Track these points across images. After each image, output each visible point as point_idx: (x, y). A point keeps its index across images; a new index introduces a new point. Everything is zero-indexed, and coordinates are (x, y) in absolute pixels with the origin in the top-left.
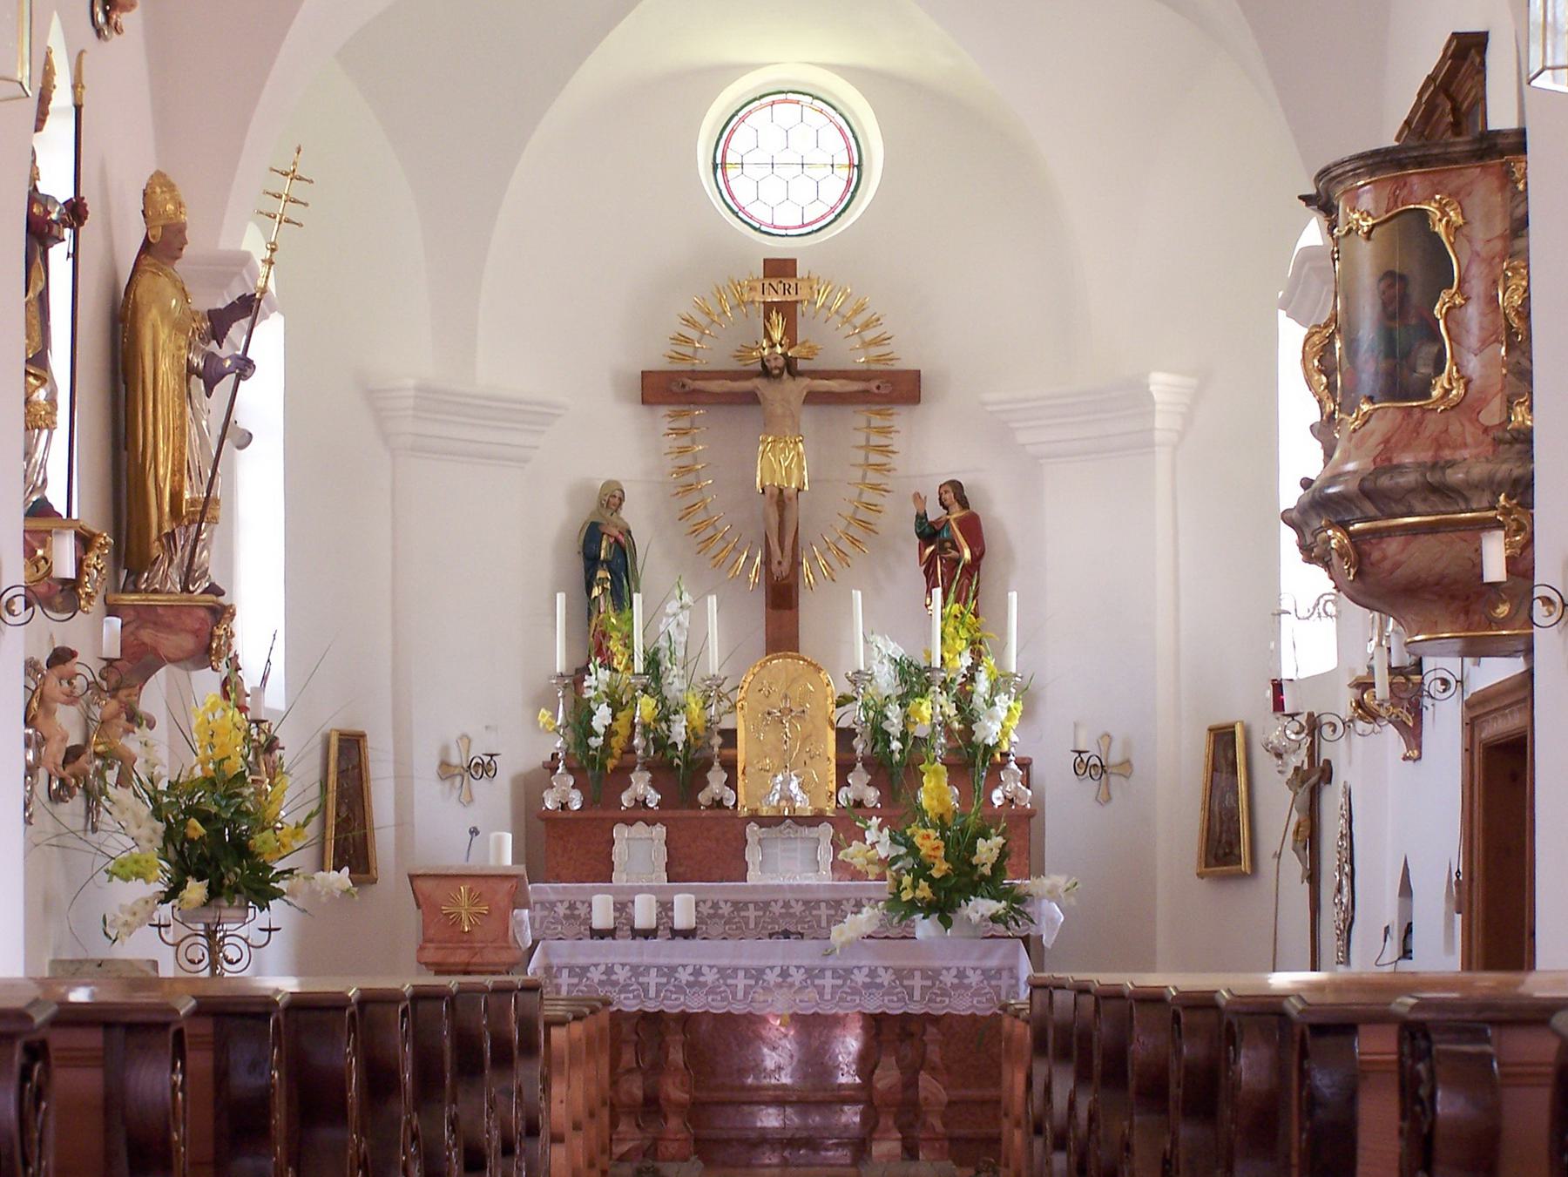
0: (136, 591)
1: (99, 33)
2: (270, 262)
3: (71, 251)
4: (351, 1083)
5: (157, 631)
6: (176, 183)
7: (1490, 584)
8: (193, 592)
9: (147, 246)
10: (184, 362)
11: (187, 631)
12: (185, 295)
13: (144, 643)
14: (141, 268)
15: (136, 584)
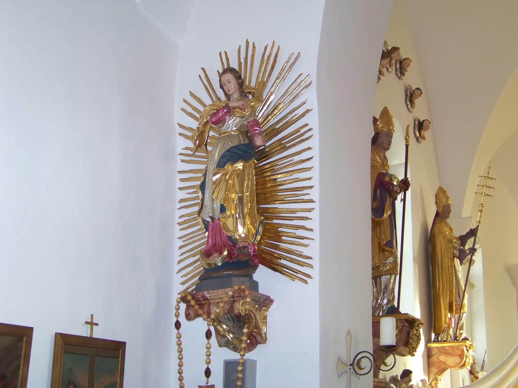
0: (438, 341)
1: (399, 78)
2: (481, 211)
3: (403, 198)
4: (455, 290)
5: (446, 356)
6: (446, 190)
7: (94, 338)
8: (458, 340)
9: (437, 214)
10: (452, 253)
11: (456, 355)
12: (452, 230)
13: (441, 361)
14: (436, 222)
15: (438, 338)
